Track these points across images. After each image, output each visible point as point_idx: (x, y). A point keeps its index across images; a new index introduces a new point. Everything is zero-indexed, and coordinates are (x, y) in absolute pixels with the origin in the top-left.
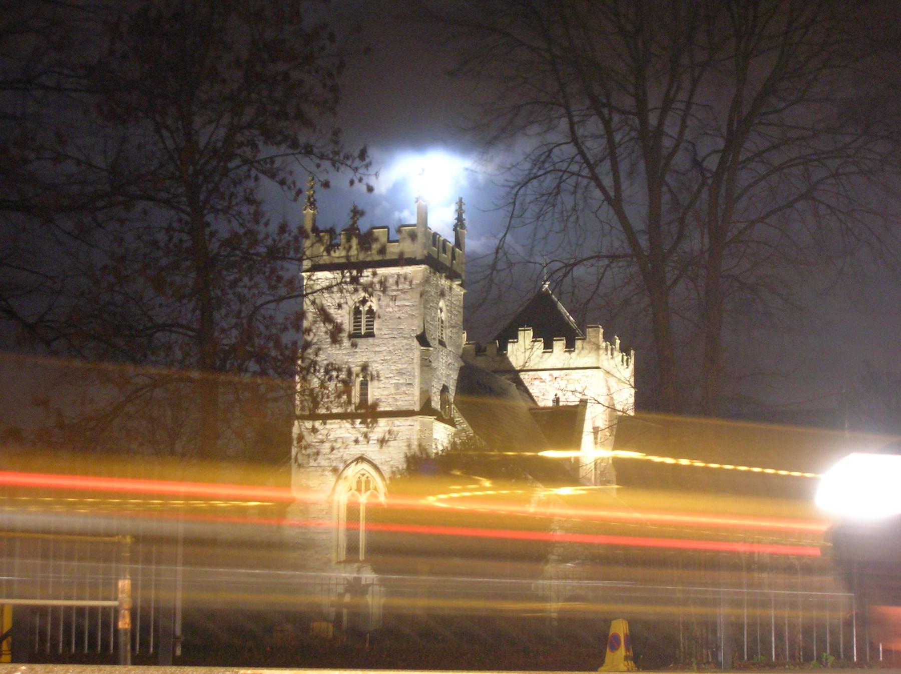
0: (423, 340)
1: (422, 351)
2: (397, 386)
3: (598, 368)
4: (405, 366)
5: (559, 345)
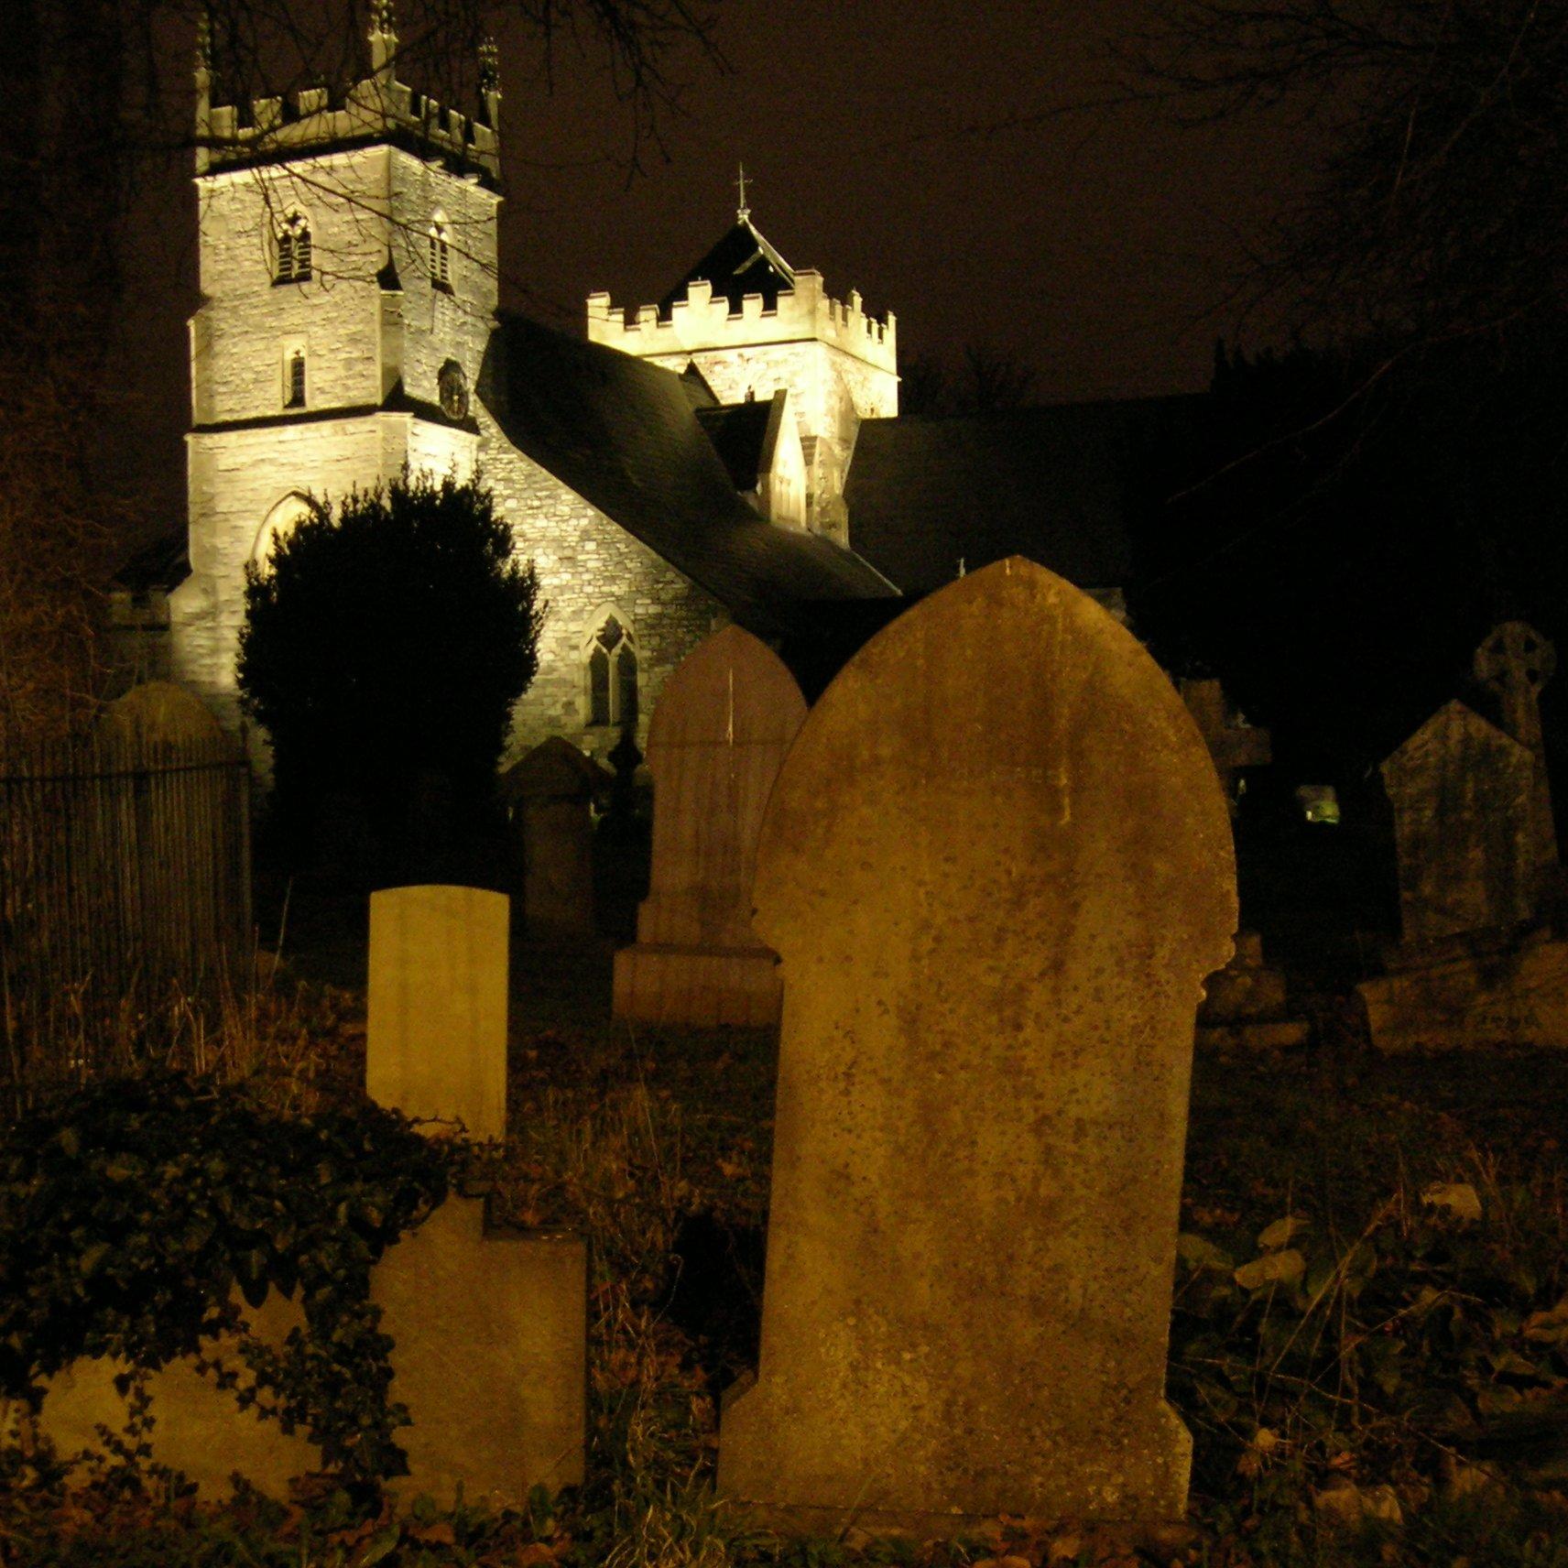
0: (388, 278)
1: (383, 298)
2: (349, 363)
3: (814, 340)
4: (360, 327)
5: (752, 305)
